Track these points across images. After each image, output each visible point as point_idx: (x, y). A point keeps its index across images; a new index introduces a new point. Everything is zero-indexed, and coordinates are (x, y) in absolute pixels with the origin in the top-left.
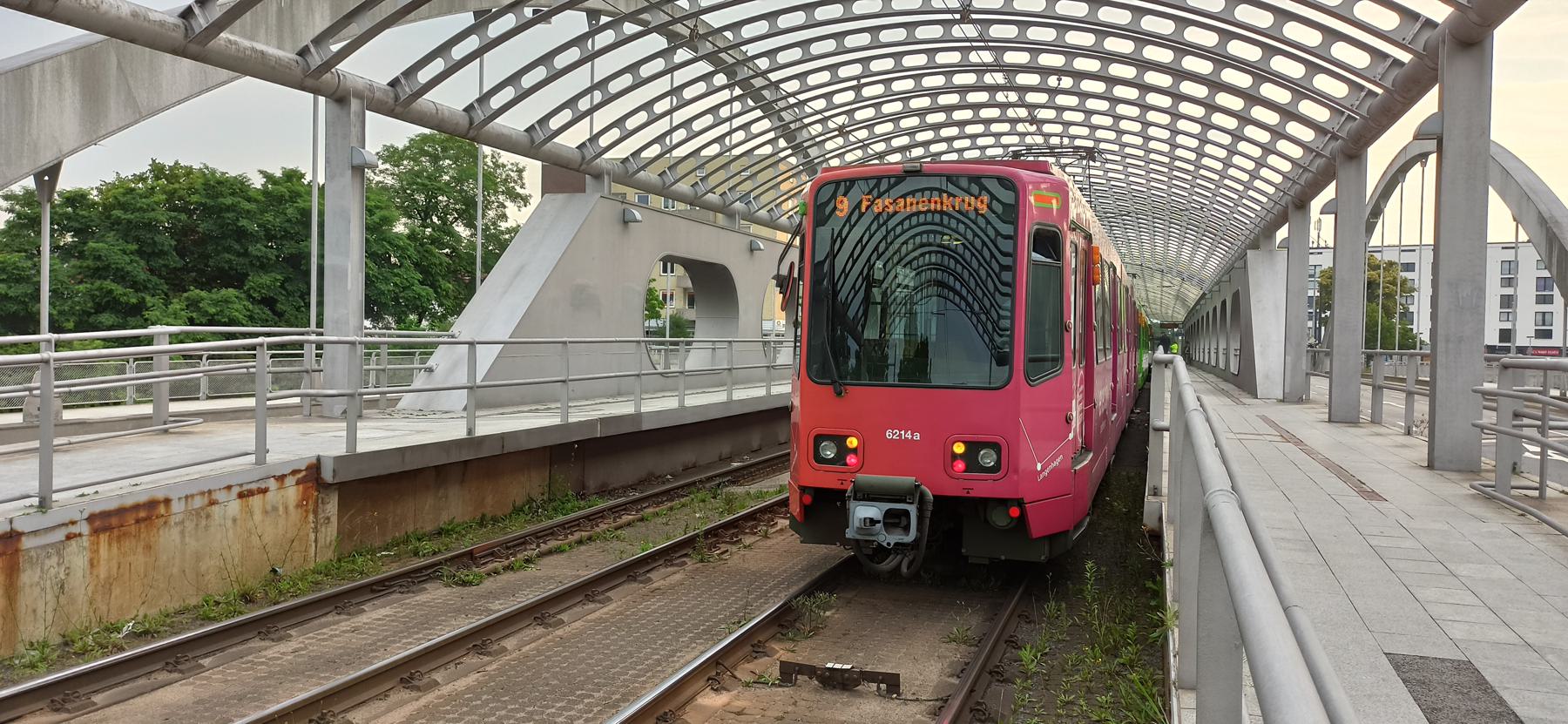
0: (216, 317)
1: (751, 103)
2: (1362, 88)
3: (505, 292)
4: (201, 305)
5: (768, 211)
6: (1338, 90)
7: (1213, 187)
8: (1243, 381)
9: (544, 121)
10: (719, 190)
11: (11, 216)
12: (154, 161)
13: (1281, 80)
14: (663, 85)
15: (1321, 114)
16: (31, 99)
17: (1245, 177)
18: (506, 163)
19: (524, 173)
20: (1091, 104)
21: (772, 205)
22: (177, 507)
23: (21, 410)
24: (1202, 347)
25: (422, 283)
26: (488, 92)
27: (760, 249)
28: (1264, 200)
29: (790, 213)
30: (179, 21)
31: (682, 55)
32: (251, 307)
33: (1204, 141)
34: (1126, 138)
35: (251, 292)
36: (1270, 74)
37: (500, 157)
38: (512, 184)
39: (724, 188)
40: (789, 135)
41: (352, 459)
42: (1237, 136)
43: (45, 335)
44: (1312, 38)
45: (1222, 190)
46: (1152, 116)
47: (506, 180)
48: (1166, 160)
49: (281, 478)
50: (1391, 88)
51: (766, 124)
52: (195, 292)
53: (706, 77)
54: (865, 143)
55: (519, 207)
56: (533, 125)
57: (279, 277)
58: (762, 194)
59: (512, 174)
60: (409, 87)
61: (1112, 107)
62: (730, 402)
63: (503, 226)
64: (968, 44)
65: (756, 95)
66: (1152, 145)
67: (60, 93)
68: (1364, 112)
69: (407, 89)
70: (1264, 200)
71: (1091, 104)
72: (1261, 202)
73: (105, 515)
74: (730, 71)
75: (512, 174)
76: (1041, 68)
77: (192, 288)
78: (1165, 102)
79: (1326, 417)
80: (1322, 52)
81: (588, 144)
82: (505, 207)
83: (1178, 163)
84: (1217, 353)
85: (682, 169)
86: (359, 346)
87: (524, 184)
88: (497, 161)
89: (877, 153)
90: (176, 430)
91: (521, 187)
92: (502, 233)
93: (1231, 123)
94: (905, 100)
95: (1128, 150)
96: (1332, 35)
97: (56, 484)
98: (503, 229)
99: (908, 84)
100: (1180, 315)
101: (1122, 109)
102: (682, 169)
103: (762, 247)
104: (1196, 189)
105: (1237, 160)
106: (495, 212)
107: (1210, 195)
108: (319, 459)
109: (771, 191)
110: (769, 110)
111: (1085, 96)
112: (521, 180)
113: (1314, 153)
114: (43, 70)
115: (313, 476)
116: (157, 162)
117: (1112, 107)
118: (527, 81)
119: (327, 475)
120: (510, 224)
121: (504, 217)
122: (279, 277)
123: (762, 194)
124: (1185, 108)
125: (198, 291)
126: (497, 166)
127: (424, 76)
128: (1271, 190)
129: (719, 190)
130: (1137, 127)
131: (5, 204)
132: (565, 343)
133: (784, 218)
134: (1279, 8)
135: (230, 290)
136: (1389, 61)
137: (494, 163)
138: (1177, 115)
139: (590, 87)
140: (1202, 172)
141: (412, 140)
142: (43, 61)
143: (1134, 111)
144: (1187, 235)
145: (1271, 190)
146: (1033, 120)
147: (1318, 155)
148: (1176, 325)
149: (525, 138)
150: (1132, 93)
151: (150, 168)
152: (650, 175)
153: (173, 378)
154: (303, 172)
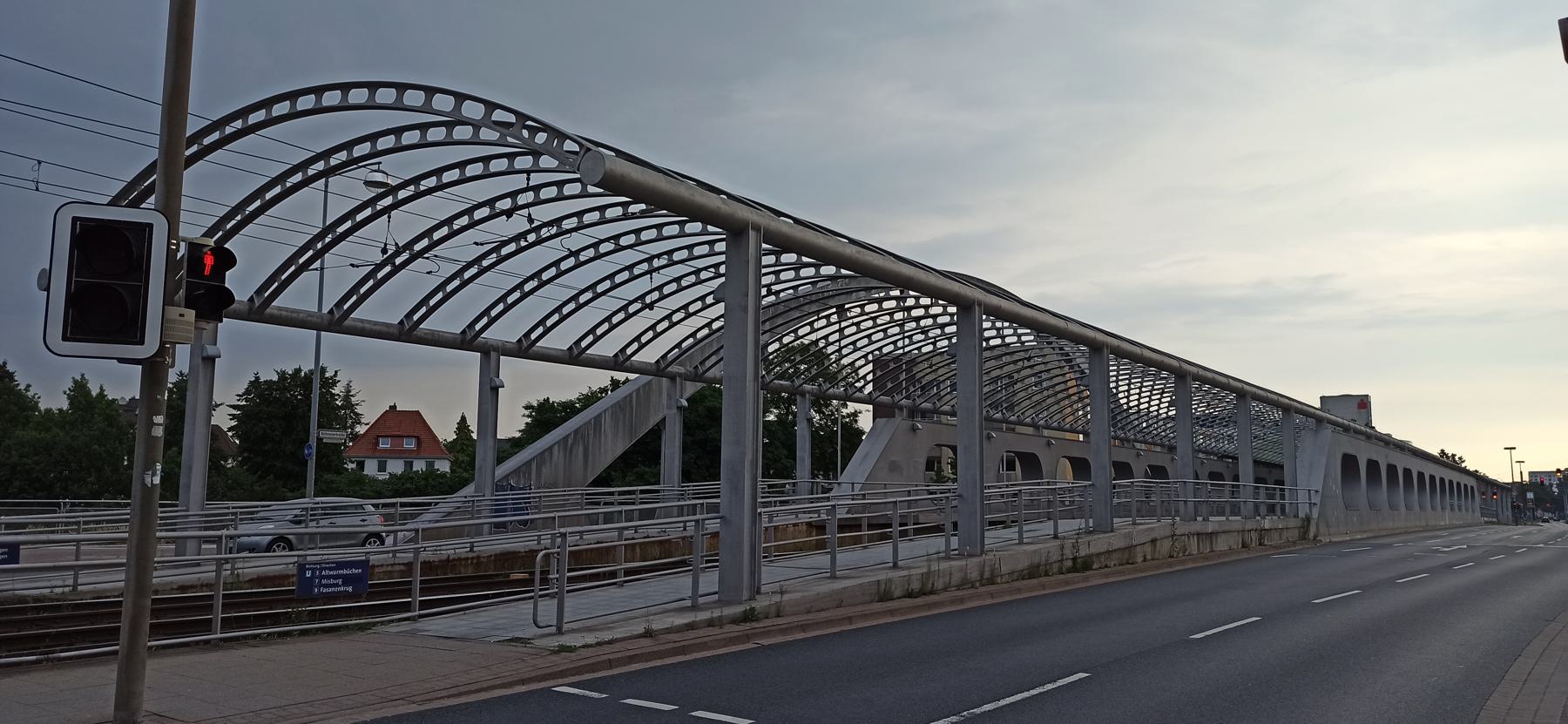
4: (646, 477)
11: (529, 420)
12: (612, 378)
25: (787, 457)
52: (643, 468)
57: (693, 456)
80: (797, 270)
92: (843, 417)
98: (844, 414)
118: (615, 320)
122: (693, 456)
125: (643, 467)
131: (527, 412)
134: (412, 239)
139: (559, 320)
146: (936, 326)
153: (338, 544)
154: (71, 384)
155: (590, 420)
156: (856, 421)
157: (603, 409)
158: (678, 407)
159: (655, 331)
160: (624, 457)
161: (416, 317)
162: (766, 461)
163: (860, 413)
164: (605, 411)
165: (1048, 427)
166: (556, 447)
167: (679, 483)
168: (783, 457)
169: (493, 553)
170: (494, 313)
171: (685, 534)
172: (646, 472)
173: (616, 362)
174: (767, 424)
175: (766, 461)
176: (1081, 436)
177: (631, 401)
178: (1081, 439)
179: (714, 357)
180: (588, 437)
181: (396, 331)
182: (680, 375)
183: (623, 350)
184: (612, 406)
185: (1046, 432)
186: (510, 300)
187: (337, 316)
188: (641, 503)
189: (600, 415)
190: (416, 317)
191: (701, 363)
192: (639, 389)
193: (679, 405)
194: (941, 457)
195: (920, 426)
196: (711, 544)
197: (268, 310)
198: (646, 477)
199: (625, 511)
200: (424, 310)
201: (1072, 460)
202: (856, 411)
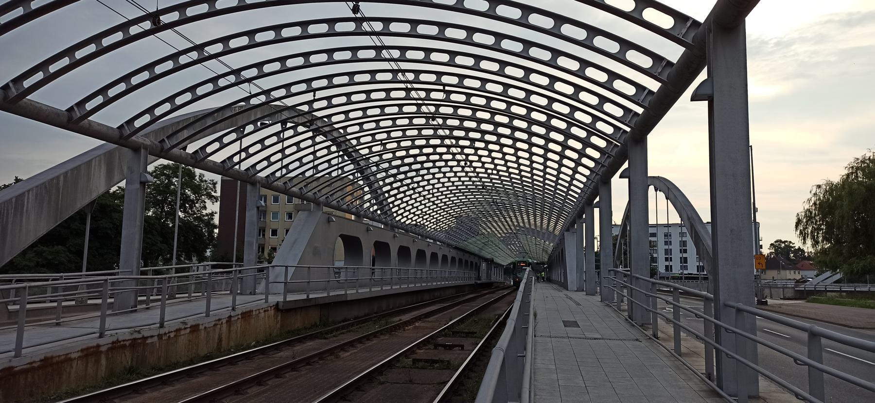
0: (52, 261)
1: (346, 158)
3: (291, 249)
5: (337, 202)
8: (564, 285)
9: (131, 121)
10: (313, 191)
13: (581, 125)
16: (91, 170)
17: (568, 179)
18: (207, 179)
19: (217, 185)
21: (339, 199)
22: (254, 313)
23: (101, 298)
24: (559, 272)
27: (333, 221)
29: (337, 200)
30: (159, 144)
31: (319, 139)
32: (70, 256)
35: (70, 247)
37: (204, 177)
38: (210, 191)
39: (316, 190)
40: (361, 170)
41: (285, 302)
47: (206, 189)
48: (553, 184)
49: (271, 307)
51: (352, 167)
53: (328, 147)
54: (367, 156)
55: (213, 202)
56: (72, 107)
58: (323, 188)
59: (210, 186)
60: (80, 112)
62: (329, 296)
63: (204, 212)
64: (425, 115)
65: (349, 155)
67: (100, 169)
69: (272, 179)
73: (246, 313)
74: (338, 145)
75: (210, 186)
77: (39, 246)
79: (600, 300)
81: (76, 108)
82: (205, 202)
84: (561, 275)
85: (295, 181)
86: (270, 267)
87: (216, 191)
88: (202, 178)
89: (384, 169)
90: (214, 297)
91: (214, 192)
92: (204, 216)
93: (575, 156)
96: (603, 99)
97: (24, 344)
98: (204, 214)
99: (409, 143)
102: (295, 181)
103: (334, 220)
106: (199, 205)
108: (278, 302)
109: (339, 192)
110: (354, 161)
112: (215, 189)
113: (601, 165)
114: (95, 161)
115: (277, 306)
116: (18, 178)
119: (281, 307)
120: (208, 211)
121: (205, 208)
123: (323, 188)
125: (42, 247)
126: (202, 181)
127: (89, 106)
128: (582, 186)
129: (313, 191)
130: (541, 160)
132: (329, 267)
133: (335, 202)
135: (60, 247)
137: (200, 180)
141: (156, 167)
142: (96, 157)
147: (597, 174)
149: (117, 133)
151: (15, 181)
152: (280, 183)
155: (11, 199)
156: (213, 219)
157: (27, 189)
158: (141, 183)
160: (47, 239)
162: (145, 245)
163: (215, 213)
164: (28, 191)
166: (152, 133)
167: (138, 268)
168: (159, 242)
171: (162, 331)
172: (45, 251)
173: (70, 119)
174: (147, 219)
175: (145, 245)
177: (58, 183)
180: (8, 215)
182: (146, 147)
184: (37, 187)
188: (65, 279)
189: (22, 195)
191: (168, 137)
192: (66, 173)
193: (143, 180)
194: (264, 244)
196: (189, 341)
197: (20, 103)
198: (44, 255)
202: (213, 212)
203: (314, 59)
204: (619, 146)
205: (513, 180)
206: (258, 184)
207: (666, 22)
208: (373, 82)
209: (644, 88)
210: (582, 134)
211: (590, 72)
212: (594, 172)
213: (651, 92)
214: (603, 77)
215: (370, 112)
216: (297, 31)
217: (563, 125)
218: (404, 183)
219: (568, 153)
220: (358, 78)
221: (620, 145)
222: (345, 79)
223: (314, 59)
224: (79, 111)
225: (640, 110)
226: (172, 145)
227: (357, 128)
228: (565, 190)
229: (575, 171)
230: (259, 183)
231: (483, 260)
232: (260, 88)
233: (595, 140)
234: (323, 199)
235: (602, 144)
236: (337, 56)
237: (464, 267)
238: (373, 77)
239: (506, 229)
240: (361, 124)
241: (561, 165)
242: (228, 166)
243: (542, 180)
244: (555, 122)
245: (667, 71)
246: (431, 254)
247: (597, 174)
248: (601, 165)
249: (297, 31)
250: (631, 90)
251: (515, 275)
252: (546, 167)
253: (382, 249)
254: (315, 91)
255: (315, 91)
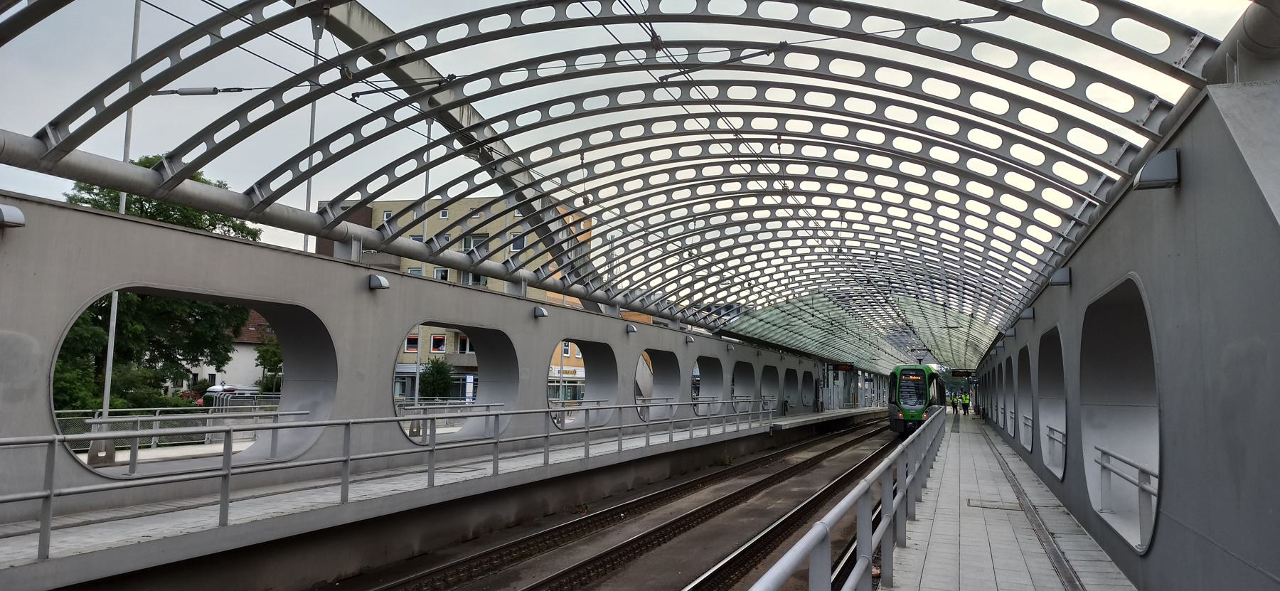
2: (1099, 174)
6: (1078, 177)
7: (1003, 269)
13: (1023, 168)
14: (576, 160)
15: (1065, 202)
17: (1008, 249)
20: (910, 187)
24: (989, 402)
26: (316, 165)
27: (692, 342)
28: (1029, 271)
33: (993, 223)
34: (943, 224)
36: (804, 159)
42: (1027, 219)
43: (105, 418)
44: (1049, 125)
45: (1011, 273)
46: (971, 205)
48: (981, 249)
50: (1127, 173)
60: (172, 170)
61: (932, 192)
66: (969, 233)
68: (1103, 198)
70: (1029, 271)
71: (910, 187)
72: (1026, 274)
76: (895, 152)
78: (987, 192)
83: (991, 254)
93: (1021, 205)
94: (831, 148)
95: (944, 236)
96: (1068, 122)
100: (973, 364)
101: (941, 195)
103: (635, 330)
104: (1007, 280)
105: (1026, 243)
107: (1000, 276)
111: (904, 178)
117: (932, 192)
124: (1007, 200)
127: (275, 185)
128: (1033, 261)
130: (955, 214)
136: (1125, 147)
138: (998, 206)
140: (1015, 264)
143: (954, 199)
144: (966, 291)
145: (1033, 261)
148: (968, 374)
150: (953, 180)
159: (825, 301)
161: (73, 127)
165: (538, 284)
169: (882, 558)
170: (219, 137)
176: (312, 240)
178: (312, 249)
179: (458, 227)
181: (240, 204)
183: (264, 183)
185: (534, 293)
186: (253, 116)
187: (53, 142)
190: (73, 127)
195: (545, 313)
197: (268, 210)
199: (141, 421)
200: (91, 113)
201: (585, 347)
203: (555, 112)
204: (1096, 206)
205: (906, 252)
206: (523, 283)
207: (1156, 42)
208: (649, 136)
209: (1150, 97)
210: (1027, 185)
211: (1040, 70)
212: (1060, 236)
213: (1164, 106)
214: (1064, 79)
215: (654, 180)
216: (521, 75)
217: (989, 170)
218: (739, 286)
219: (1007, 200)
220: (626, 133)
221: (1098, 204)
222: (607, 136)
223: (555, 112)
224: (332, 212)
225: (1141, 141)
226: (337, 216)
227: (639, 205)
228: (1005, 260)
229: (1021, 234)
230: (525, 280)
231: (831, 367)
232: (217, 6)
233: (1049, 195)
234: (526, 272)
235: (1065, 202)
236: (589, 104)
237: (800, 386)
238: (648, 129)
239: (884, 320)
240: (644, 199)
241: (993, 223)
242: (389, 235)
243: (957, 240)
244: (974, 165)
245: (1161, 117)
246: (804, 374)
247: (1065, 240)
248: (1073, 222)
249: (521, 75)
250: (1123, 103)
251: (895, 403)
252: (964, 227)
253: (709, 365)
254: (582, 166)
255: (582, 166)
